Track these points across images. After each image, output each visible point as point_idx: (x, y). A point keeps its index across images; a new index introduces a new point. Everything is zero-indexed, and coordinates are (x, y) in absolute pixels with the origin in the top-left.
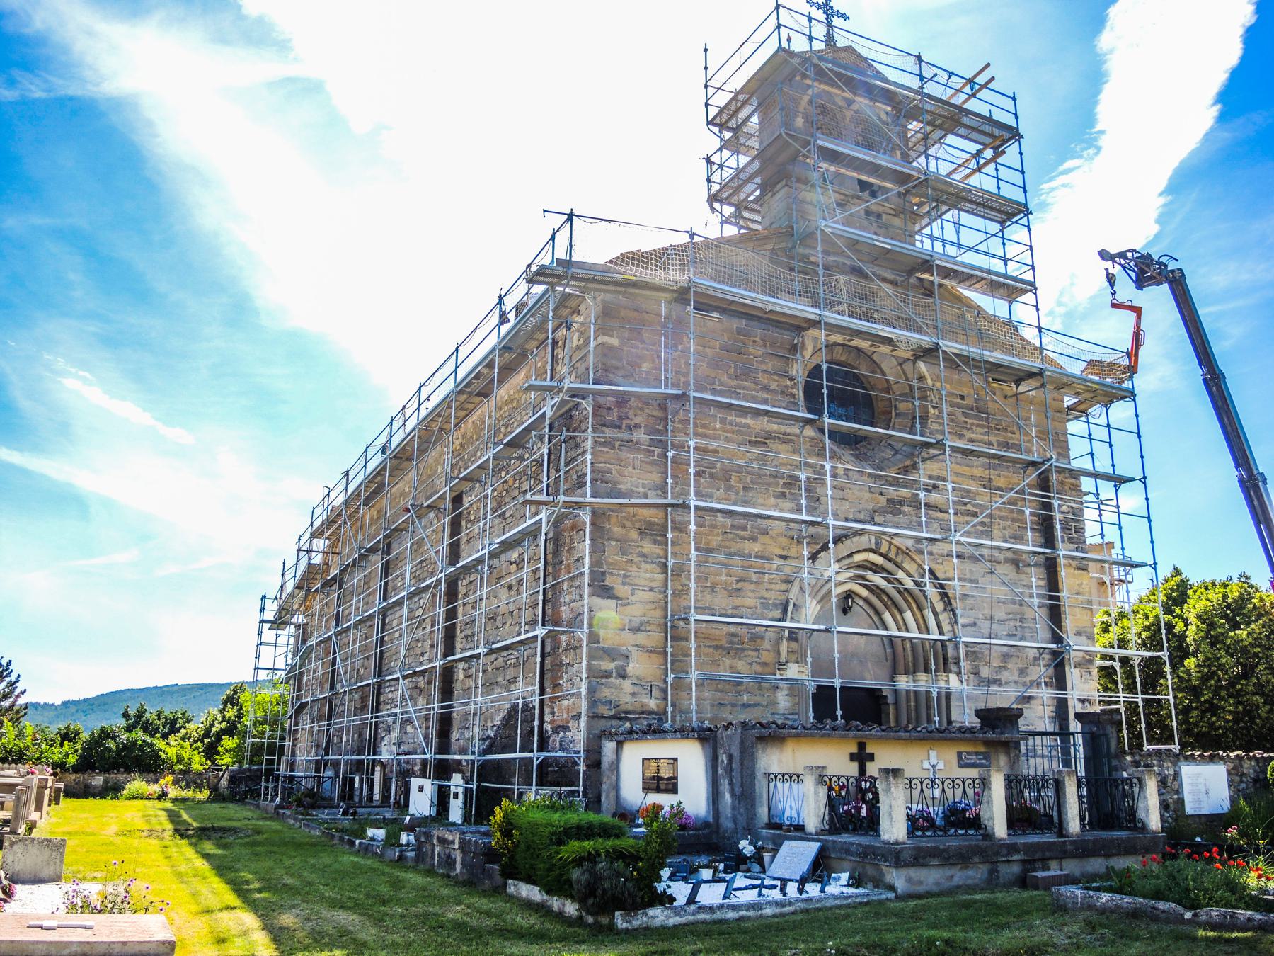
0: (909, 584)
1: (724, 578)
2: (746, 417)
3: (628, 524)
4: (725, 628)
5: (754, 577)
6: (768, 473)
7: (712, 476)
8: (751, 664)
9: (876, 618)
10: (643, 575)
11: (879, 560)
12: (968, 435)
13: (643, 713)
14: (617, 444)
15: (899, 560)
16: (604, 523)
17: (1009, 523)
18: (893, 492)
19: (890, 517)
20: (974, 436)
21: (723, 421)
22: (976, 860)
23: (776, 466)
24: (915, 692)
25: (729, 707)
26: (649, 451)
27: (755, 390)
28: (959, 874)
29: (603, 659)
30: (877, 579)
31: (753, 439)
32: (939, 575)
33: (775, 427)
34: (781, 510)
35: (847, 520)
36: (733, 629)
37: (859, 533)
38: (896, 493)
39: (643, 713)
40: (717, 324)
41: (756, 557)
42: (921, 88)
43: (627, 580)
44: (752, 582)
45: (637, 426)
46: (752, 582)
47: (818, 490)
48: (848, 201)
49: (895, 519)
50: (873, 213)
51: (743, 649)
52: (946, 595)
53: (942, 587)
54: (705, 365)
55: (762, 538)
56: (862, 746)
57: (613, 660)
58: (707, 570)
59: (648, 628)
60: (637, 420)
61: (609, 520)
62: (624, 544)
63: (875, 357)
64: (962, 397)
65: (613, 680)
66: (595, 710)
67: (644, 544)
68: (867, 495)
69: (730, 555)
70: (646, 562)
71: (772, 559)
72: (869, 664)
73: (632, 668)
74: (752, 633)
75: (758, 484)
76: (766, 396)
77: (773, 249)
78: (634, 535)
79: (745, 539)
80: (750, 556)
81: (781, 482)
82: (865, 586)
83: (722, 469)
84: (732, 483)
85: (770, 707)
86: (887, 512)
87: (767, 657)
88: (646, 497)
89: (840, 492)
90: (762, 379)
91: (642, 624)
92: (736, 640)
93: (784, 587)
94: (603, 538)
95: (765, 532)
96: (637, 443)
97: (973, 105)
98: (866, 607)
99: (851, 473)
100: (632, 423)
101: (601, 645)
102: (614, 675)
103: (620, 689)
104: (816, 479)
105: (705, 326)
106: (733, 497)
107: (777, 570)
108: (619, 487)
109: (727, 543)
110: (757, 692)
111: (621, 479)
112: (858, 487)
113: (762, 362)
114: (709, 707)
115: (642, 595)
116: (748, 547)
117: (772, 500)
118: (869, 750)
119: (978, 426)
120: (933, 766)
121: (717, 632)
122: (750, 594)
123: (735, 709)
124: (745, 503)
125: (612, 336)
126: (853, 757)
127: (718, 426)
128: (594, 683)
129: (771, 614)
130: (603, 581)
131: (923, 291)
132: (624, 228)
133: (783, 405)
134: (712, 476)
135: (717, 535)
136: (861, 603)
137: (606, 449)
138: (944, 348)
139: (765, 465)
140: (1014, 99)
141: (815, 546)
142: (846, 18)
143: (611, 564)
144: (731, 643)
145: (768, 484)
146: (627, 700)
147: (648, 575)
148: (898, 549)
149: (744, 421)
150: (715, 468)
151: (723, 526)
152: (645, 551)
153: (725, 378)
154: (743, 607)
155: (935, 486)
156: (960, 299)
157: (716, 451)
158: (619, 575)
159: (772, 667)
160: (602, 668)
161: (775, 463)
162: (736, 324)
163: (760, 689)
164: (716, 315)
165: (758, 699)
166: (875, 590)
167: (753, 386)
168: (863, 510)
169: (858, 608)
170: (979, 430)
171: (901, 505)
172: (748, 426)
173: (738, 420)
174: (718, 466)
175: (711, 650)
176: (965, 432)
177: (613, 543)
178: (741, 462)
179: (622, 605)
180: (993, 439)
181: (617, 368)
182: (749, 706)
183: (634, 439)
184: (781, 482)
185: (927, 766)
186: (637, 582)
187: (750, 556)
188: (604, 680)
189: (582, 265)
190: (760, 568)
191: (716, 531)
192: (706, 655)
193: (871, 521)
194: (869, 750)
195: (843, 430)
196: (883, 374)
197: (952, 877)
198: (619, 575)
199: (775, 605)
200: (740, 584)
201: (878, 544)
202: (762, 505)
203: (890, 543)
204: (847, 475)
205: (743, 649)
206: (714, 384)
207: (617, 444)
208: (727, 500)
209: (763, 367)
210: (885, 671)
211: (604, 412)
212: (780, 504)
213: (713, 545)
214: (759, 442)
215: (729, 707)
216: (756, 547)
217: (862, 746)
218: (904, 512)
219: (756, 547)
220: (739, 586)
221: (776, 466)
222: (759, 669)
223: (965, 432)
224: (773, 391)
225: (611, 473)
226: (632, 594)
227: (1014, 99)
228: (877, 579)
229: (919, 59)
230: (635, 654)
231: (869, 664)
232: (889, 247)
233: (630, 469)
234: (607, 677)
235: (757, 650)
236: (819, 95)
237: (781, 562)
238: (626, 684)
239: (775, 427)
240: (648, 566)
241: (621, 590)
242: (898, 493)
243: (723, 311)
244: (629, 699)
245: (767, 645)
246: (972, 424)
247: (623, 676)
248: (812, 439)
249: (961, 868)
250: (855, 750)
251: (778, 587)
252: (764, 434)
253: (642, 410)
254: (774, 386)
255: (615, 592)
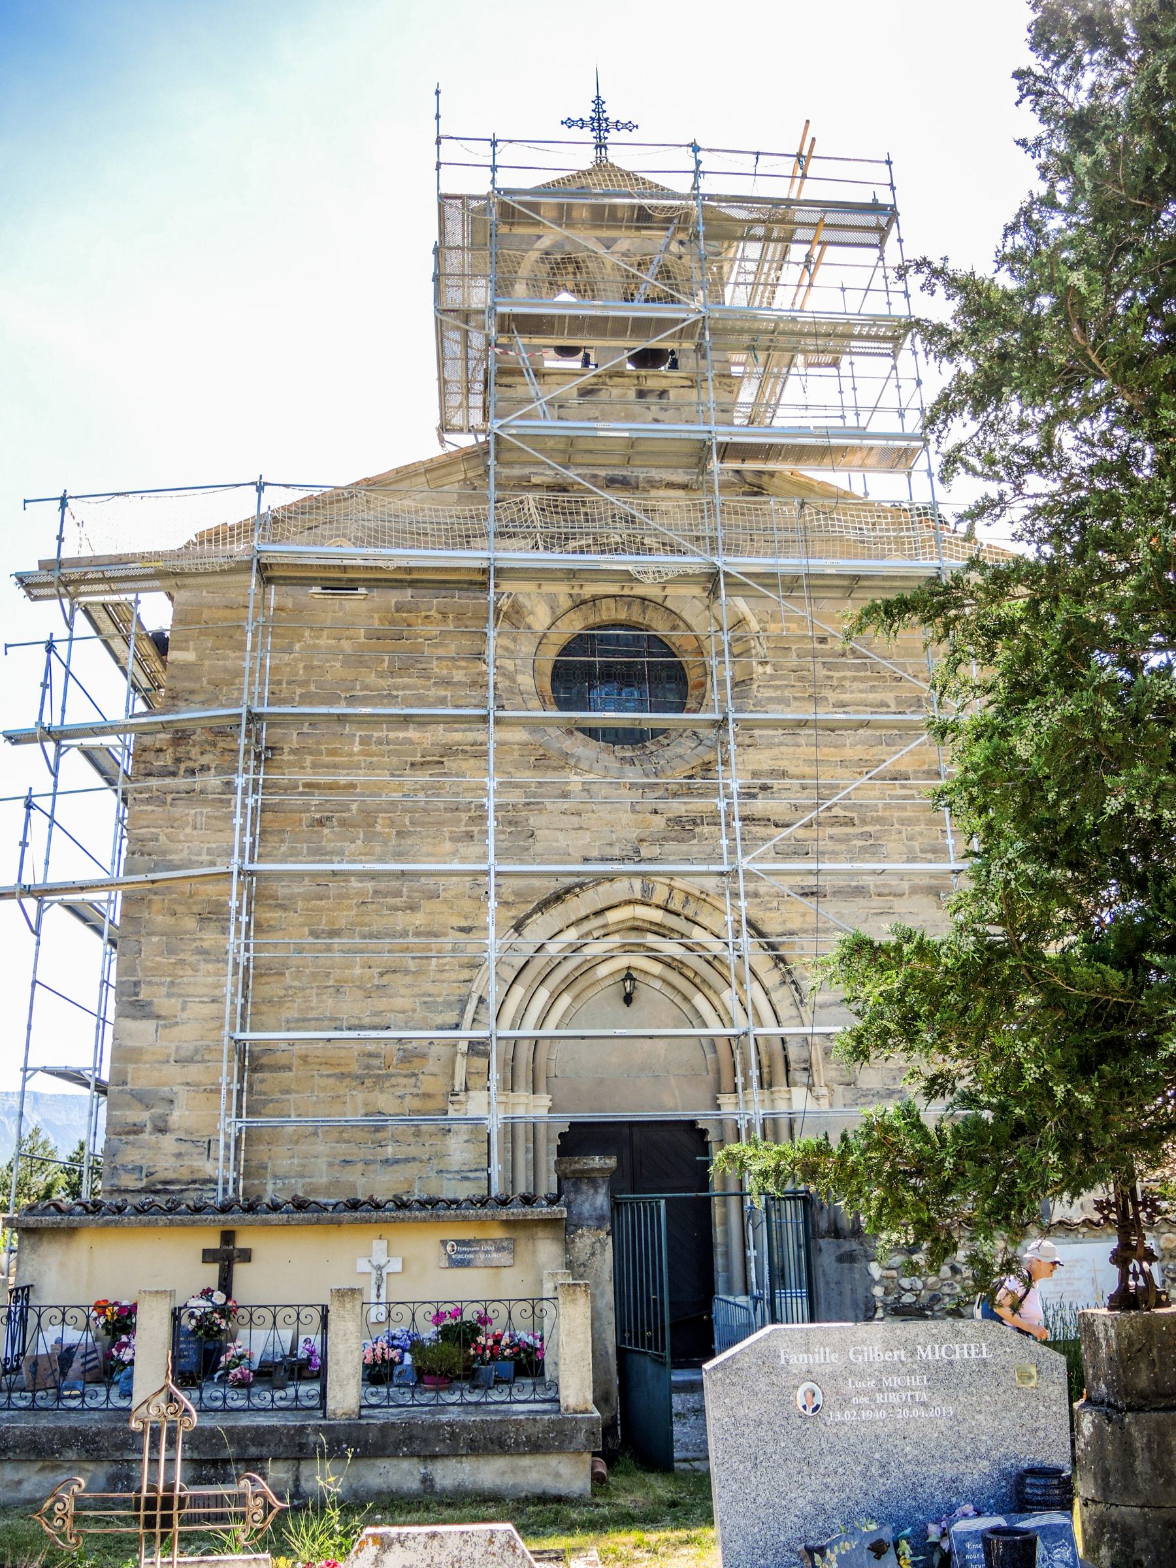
0: (716, 947)
1: (358, 971)
2: (407, 730)
3: (180, 909)
4: (357, 1047)
5: (412, 965)
6: (442, 806)
7: (343, 823)
8: (401, 1097)
9: (685, 1007)
10: (200, 979)
11: (657, 916)
12: (832, 696)
13: (194, 1182)
14: (169, 798)
15: (689, 912)
16: (140, 912)
17: (922, 827)
18: (678, 807)
19: (670, 846)
20: (845, 697)
21: (364, 741)
22: (71, 1454)
23: (456, 794)
24: (774, 1120)
25: (360, 1166)
26: (221, 801)
27: (423, 687)
28: (36, 1479)
29: (128, 1106)
30: (670, 948)
31: (419, 759)
32: (766, 929)
33: (458, 737)
34: (464, 859)
35: (586, 860)
36: (371, 1047)
37: (610, 878)
38: (683, 808)
39: (194, 1182)
40: (364, 604)
41: (417, 934)
42: (695, 187)
43: (175, 990)
44: (407, 972)
45: (204, 768)
46: (407, 972)
47: (531, 821)
48: (604, 384)
49: (684, 847)
50: (652, 391)
51: (389, 1076)
52: (781, 959)
53: (772, 947)
54: (338, 665)
55: (427, 905)
56: (228, 1237)
57: (148, 1107)
58: (329, 962)
59: (207, 1057)
60: (205, 760)
61: (149, 907)
62: (173, 941)
63: (668, 604)
64: (823, 640)
65: (145, 1136)
66: (116, 1182)
67: (206, 935)
68: (627, 817)
69: (371, 936)
70: (207, 961)
71: (446, 935)
72: (673, 1081)
73: (178, 1117)
74: (405, 1050)
75: (423, 824)
76: (443, 693)
77: (465, 480)
78: (190, 923)
79: (397, 909)
80: (404, 934)
81: (464, 816)
82: (656, 959)
83: (361, 811)
84: (378, 828)
85: (435, 1161)
86: (665, 839)
87: (428, 1084)
88: (212, 864)
89: (575, 819)
90: (439, 669)
91: (196, 1051)
92: (375, 1062)
93: (466, 974)
94: (138, 933)
95: (434, 895)
96: (202, 792)
97: (812, 191)
98: (668, 991)
99: (594, 788)
100: (197, 765)
101: (129, 1087)
102: (149, 1128)
103: (157, 1148)
104: (528, 804)
105: (341, 609)
106: (378, 849)
107: (453, 950)
108: (169, 857)
109: (367, 919)
110: (412, 1139)
111: (172, 846)
112: (609, 807)
113: (436, 646)
114: (324, 1167)
115: (197, 1009)
116: (402, 920)
117: (448, 846)
118: (241, 1243)
119: (855, 679)
120: (379, 1268)
121: (343, 1053)
122: (403, 991)
123: (371, 1167)
124: (399, 856)
125: (187, 649)
126: (208, 1256)
127: (356, 750)
128: (116, 1143)
129: (439, 1020)
130: (137, 994)
131: (747, 488)
132: (150, 501)
133: (474, 701)
134: (343, 823)
135: (349, 908)
136: (658, 984)
137: (150, 808)
138: (727, 569)
139: (438, 795)
140: (889, 162)
141: (524, 907)
142: (630, 126)
143: (151, 969)
144: (368, 1067)
145: (441, 823)
146: (167, 1165)
147: (210, 980)
148: (688, 894)
149: (401, 735)
150: (349, 810)
151: (360, 893)
152: (206, 945)
153: (372, 679)
154: (392, 1011)
155: (764, 788)
156: (808, 487)
157: (352, 786)
158: (162, 984)
159: (440, 1099)
160: (129, 1120)
161: (455, 789)
162: (395, 597)
163: (417, 1134)
164: (362, 590)
165: (413, 1151)
166: (670, 963)
167: (422, 682)
168: (619, 840)
169: (650, 994)
170: (857, 685)
171: (695, 824)
172: (410, 742)
173: (392, 735)
174: (354, 807)
175: (332, 1081)
176: (827, 693)
177: (155, 939)
178: (396, 796)
179: (165, 1026)
180: (889, 697)
181: (192, 692)
182: (397, 1162)
183: (197, 787)
184: (464, 816)
185: (367, 1268)
186: (190, 990)
187: (404, 934)
188: (131, 1137)
189: (77, 562)
190: (423, 950)
191: (346, 902)
192: (323, 1089)
193: (635, 856)
194: (241, 1243)
195: (620, 725)
196: (689, 627)
197: (20, 1482)
198: (162, 984)
199: (448, 1005)
200: (386, 977)
201: (647, 891)
202: (429, 855)
203: (671, 889)
204: (588, 791)
205: (389, 1076)
206: (353, 689)
207: (169, 798)
208: (368, 854)
209: (441, 652)
210: (703, 1094)
211: (150, 756)
212: (461, 850)
213: (342, 923)
214: (429, 763)
215: (360, 1166)
216: (418, 919)
217: (228, 1237)
218: (701, 835)
219: (418, 919)
220: (385, 979)
221: (456, 794)
222: (417, 1103)
223: (827, 693)
224: (460, 684)
225: (157, 840)
226: (183, 1009)
227: (889, 162)
228: (670, 948)
229: (695, 148)
230: (183, 1095)
231: (673, 1081)
232: (627, 434)
233: (188, 830)
234: (135, 1133)
235: (414, 1075)
236: (557, 245)
237: (462, 936)
238: (168, 1142)
239: (458, 737)
240: (210, 967)
241: (164, 1004)
242: (689, 807)
243: (372, 584)
244: (171, 1162)
245: (432, 1066)
246: (844, 678)
247: (162, 1130)
248: (524, 744)
249: (42, 1469)
250: (214, 1243)
251: (453, 976)
252: (439, 750)
253: (214, 745)
254: (458, 676)
255: (156, 1009)
